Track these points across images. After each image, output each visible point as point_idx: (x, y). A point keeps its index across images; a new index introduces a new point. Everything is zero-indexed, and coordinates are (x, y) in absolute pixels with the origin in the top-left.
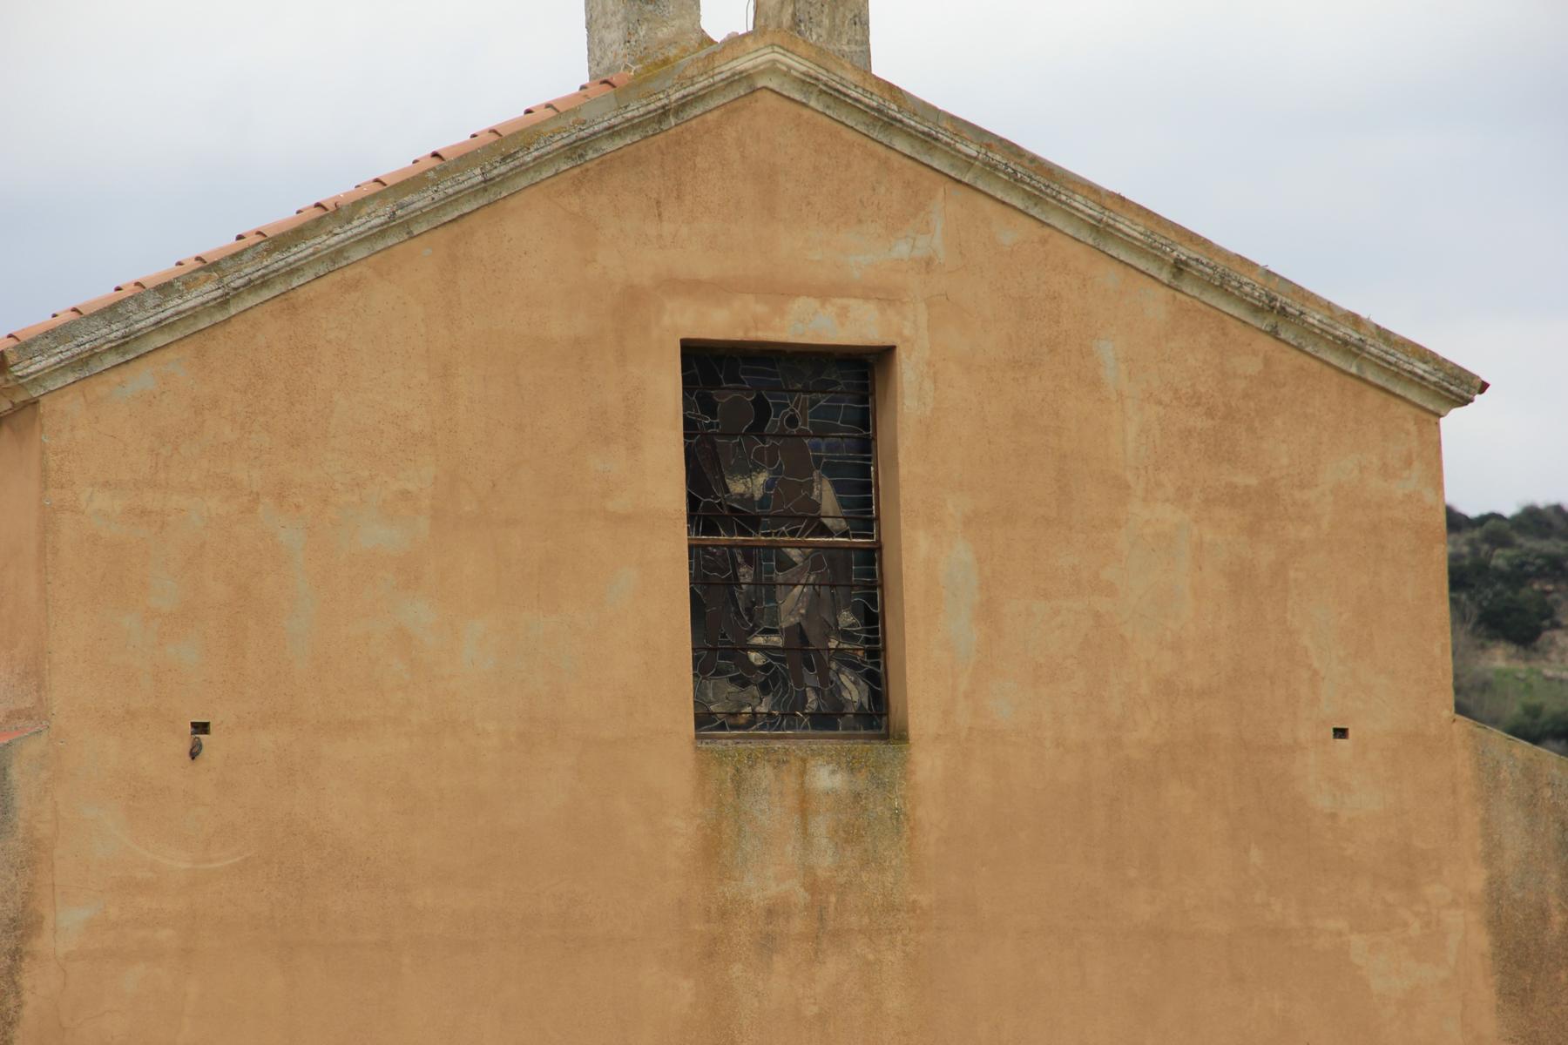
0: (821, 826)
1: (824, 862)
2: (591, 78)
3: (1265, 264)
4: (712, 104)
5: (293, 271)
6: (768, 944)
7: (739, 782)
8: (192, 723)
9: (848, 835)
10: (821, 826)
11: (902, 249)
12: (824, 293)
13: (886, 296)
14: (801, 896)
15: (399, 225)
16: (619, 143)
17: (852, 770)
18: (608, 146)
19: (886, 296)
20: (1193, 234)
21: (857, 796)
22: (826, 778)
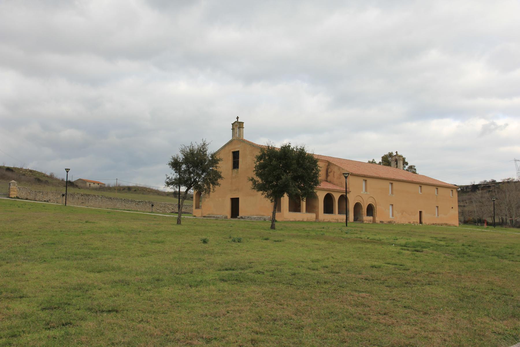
13: (239, 148)
22: (236, 171)
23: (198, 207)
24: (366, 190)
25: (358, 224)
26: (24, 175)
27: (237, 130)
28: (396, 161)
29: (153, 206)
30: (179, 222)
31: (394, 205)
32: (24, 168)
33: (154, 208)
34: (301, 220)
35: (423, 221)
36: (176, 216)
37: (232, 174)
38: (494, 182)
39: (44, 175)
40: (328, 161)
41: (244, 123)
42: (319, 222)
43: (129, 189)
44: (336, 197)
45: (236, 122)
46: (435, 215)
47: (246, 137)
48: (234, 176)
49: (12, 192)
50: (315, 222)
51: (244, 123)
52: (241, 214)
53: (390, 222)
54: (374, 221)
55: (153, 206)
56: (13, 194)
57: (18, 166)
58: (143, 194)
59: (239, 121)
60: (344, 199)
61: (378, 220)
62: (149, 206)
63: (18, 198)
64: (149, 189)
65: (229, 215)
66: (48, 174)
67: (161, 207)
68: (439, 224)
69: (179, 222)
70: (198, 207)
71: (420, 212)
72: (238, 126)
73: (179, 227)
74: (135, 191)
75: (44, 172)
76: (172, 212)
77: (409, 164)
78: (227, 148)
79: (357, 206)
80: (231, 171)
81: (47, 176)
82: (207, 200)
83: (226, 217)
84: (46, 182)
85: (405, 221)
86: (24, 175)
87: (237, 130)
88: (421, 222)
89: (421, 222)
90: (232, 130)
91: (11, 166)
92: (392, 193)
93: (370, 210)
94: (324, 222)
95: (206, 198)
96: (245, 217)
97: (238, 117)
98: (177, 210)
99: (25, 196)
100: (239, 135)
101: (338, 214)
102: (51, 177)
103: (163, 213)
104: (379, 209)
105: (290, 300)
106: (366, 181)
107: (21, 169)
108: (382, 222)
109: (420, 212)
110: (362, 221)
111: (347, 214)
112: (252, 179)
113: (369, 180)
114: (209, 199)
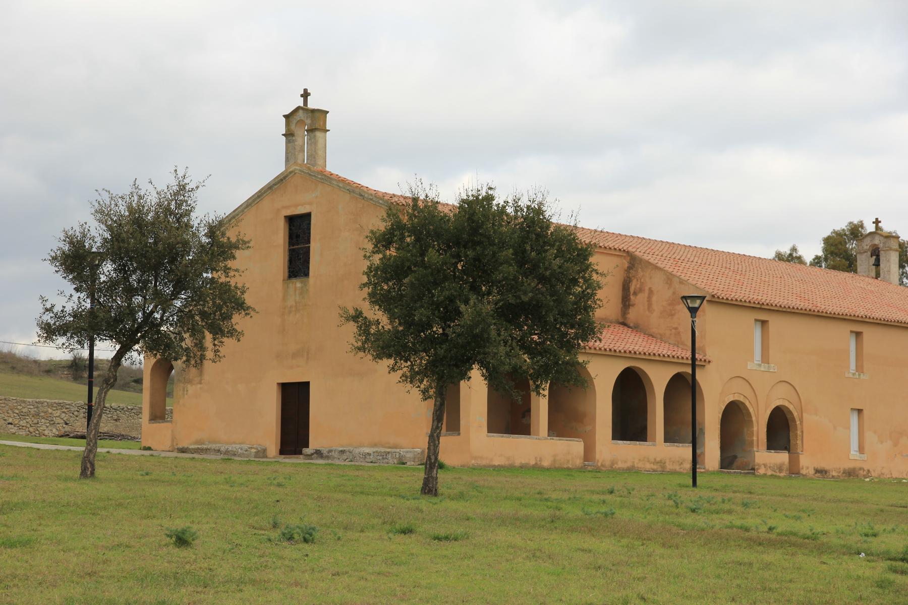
0: (297, 292)
1: (297, 298)
2: (825, 250)
3: (775, 253)
4: (289, 177)
5: (238, 215)
6: (290, 312)
7: (288, 287)
8: (308, 216)
9: (301, 294)
10: (297, 292)
11: (314, 195)
12: (302, 205)
13: (310, 203)
14: (294, 304)
15: (247, 206)
16: (277, 186)
17: (302, 283)
18: (276, 187)
19: (310, 203)
20: (259, 191)
21: (302, 287)
22: (298, 285)
23: (159, 415)
24: (765, 358)
25: (736, 480)
27: (302, 138)
30: (88, 469)
31: (865, 412)
34: (532, 462)
36: (80, 447)
37: (284, 298)
41: (328, 112)
42: (598, 470)
45: (298, 108)
47: (332, 167)
48: (291, 302)
50: (582, 469)
51: (328, 112)
52: (316, 441)
54: (794, 470)
59: (311, 105)
61: (807, 462)
65: (272, 443)
67: (22, 415)
69: (88, 469)
70: (159, 415)
76: (66, 435)
78: (266, 203)
80: (279, 284)
82: (191, 389)
87: (302, 138)
90: (284, 138)
92: (860, 368)
95: (190, 382)
96: (330, 451)
97: (305, 90)
98: (80, 426)
100: (312, 156)
106: (764, 323)
108: (821, 472)
112: (357, 316)
114: (199, 386)
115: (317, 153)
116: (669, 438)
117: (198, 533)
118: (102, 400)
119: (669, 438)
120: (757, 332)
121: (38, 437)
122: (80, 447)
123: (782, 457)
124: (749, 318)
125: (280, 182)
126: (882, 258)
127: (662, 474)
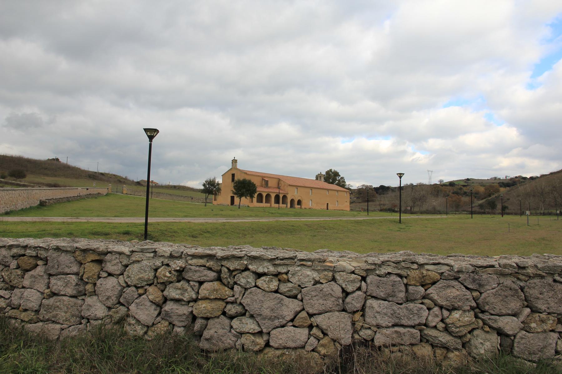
23: (215, 200)
24: (297, 193)
25: (292, 209)
26: (111, 178)
27: (234, 163)
28: (320, 177)
29: (192, 199)
30: (206, 205)
32: (110, 173)
33: (193, 200)
35: (329, 208)
36: (204, 204)
38: (412, 185)
39: (122, 178)
40: (279, 178)
42: (272, 208)
43: (175, 187)
44: (281, 196)
46: (336, 205)
47: (238, 167)
49: (124, 191)
50: (270, 208)
53: (310, 208)
54: (301, 208)
55: (192, 199)
56: (125, 192)
57: (107, 172)
58: (184, 190)
60: (285, 197)
61: (303, 207)
62: (190, 199)
63: (127, 194)
64: (188, 187)
65: (230, 204)
66: (124, 177)
67: (197, 199)
68: (338, 210)
69: (206, 205)
70: (215, 200)
71: (328, 204)
72: (234, 161)
73: (206, 207)
74: (179, 188)
75: (122, 176)
76: (203, 202)
77: (341, 176)
78: (229, 172)
79: (292, 201)
80: (231, 183)
81: (124, 179)
82: (219, 196)
83: (228, 205)
84: (124, 183)
85: (318, 208)
86: (111, 178)
87: (234, 163)
88: (327, 209)
89: (327, 209)
91: (103, 172)
92: (312, 194)
93: (299, 202)
94: (274, 208)
98: (205, 201)
99: (130, 193)
100: (235, 166)
101: (265, 203)
102: (126, 179)
103: (198, 202)
104: (304, 202)
105: (405, 364)
106: (297, 188)
107: (109, 174)
108: (305, 208)
109: (328, 204)
110: (295, 208)
111: (287, 204)
112: (232, 191)
113: (298, 188)
115: (236, 166)
116: (283, 203)
117: (248, 317)
118: (208, 197)
119: (283, 203)
120: (296, 189)
121: (199, 203)
122: (204, 204)
123: (300, 206)
124: (295, 188)
125: (231, 169)
126: (277, 185)
127: (400, 231)
